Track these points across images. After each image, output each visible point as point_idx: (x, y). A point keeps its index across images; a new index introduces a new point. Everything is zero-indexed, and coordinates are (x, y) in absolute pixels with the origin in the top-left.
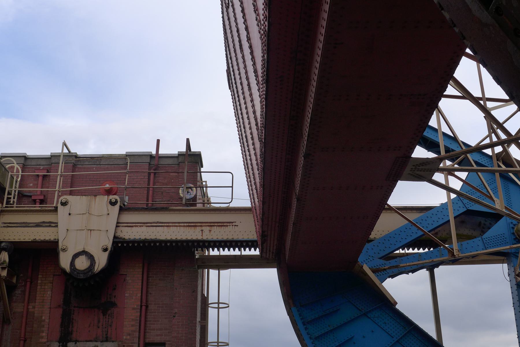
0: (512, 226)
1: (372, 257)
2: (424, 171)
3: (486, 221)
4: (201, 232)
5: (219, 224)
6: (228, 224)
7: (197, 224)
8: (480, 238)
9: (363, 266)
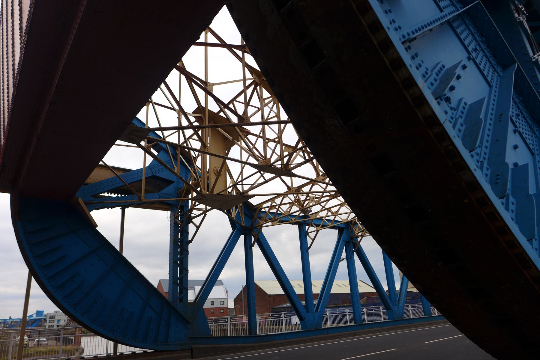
0: (177, 189)
1: (86, 194)
8: (157, 193)
9: (78, 199)
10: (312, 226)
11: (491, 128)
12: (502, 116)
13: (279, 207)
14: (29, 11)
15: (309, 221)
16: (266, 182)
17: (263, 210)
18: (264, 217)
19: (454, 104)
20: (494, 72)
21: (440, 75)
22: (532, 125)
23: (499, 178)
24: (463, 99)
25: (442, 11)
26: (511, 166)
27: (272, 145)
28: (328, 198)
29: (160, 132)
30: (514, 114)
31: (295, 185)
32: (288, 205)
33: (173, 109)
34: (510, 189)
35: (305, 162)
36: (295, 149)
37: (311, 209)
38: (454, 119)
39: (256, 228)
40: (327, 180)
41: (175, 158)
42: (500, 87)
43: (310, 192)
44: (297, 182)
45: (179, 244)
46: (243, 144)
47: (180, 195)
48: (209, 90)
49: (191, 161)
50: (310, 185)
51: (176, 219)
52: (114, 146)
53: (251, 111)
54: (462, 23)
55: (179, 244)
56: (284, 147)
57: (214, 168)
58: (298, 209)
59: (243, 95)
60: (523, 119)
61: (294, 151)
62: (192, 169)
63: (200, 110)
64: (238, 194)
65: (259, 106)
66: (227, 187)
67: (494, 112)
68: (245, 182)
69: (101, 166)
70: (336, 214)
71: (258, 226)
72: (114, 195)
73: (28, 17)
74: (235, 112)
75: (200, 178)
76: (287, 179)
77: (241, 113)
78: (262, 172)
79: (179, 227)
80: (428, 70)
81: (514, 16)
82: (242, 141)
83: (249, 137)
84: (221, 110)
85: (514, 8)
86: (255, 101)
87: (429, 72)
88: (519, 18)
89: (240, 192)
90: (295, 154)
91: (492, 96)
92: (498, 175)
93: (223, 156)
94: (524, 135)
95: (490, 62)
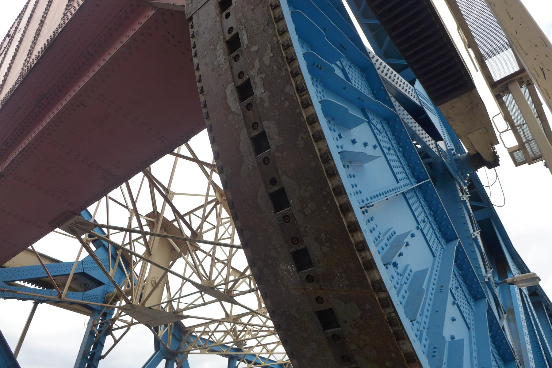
0: (106, 292)
2: (79, 229)
3: (90, 284)
8: (82, 293)
10: (243, 361)
11: (432, 297)
12: (443, 288)
13: (212, 334)
14: (13, 86)
15: (241, 356)
16: (205, 304)
17: (194, 334)
18: (193, 342)
19: (400, 270)
20: (438, 244)
21: (391, 240)
22: (470, 299)
23: (436, 351)
24: (410, 265)
25: (398, 182)
26: (448, 339)
27: (219, 266)
28: (266, 333)
29: (107, 229)
30: (454, 287)
31: (235, 313)
32: (223, 334)
33: (127, 207)
34: (446, 363)
35: (250, 291)
36: (242, 275)
37: (246, 342)
38: (399, 285)
39: (181, 353)
40: (268, 315)
41: (114, 259)
42: (442, 259)
43: (248, 324)
44: (237, 310)
45: (89, 357)
46: (190, 260)
47: (107, 300)
48: (169, 199)
49: (129, 264)
50: (251, 316)
51: (94, 327)
52: (52, 233)
53: (206, 226)
54: (414, 196)
55: (89, 357)
56: (231, 270)
57: (153, 278)
58: (232, 340)
59: (202, 209)
60: (462, 292)
61: (240, 277)
62: (129, 275)
63: (154, 215)
64: (171, 311)
65: (215, 224)
66: (162, 302)
67: (436, 282)
68: (182, 300)
69: (29, 250)
70: (271, 352)
71: (184, 352)
72: (32, 285)
73: (9, 91)
74: (189, 226)
75: (134, 285)
76: (227, 305)
77: (195, 227)
78: (203, 293)
79: (96, 337)
80: (380, 234)
81: (458, 195)
82: (189, 255)
83: (198, 252)
84: (176, 220)
85: (460, 188)
86: (212, 218)
87: (381, 236)
88: (462, 197)
89: (175, 310)
90: (241, 280)
91: (436, 266)
92: (435, 348)
93: (166, 268)
94: (462, 308)
95: (436, 234)
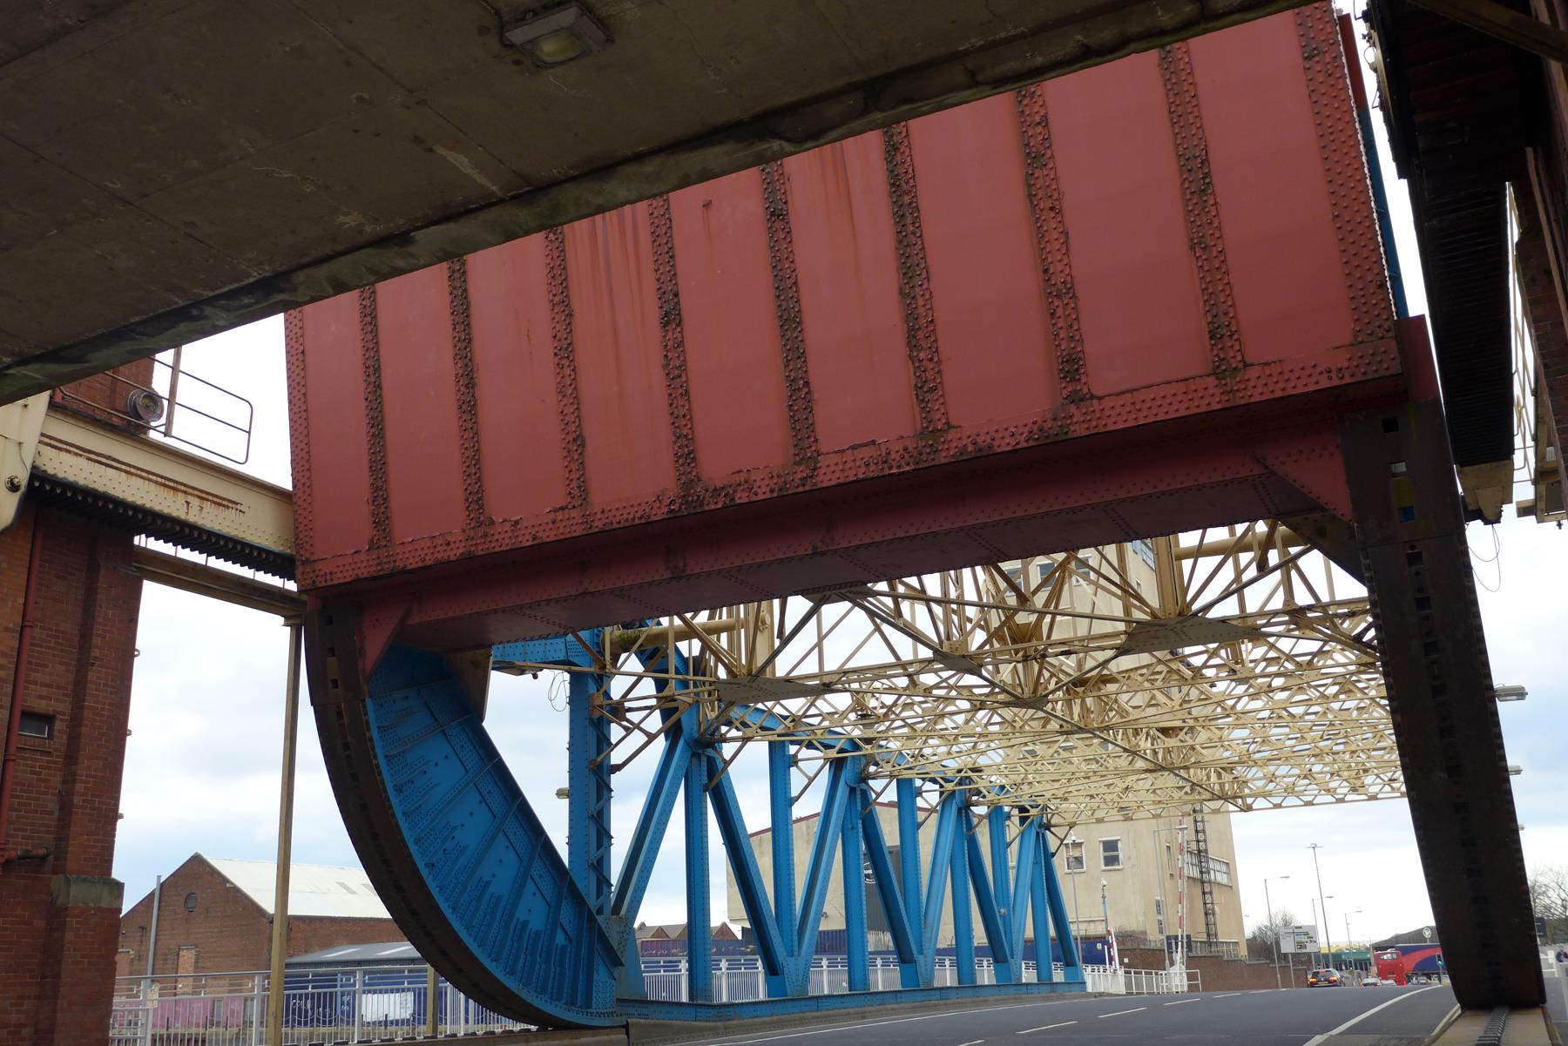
4: (185, 505)
5: (215, 499)
6: (230, 505)
7: (179, 487)
